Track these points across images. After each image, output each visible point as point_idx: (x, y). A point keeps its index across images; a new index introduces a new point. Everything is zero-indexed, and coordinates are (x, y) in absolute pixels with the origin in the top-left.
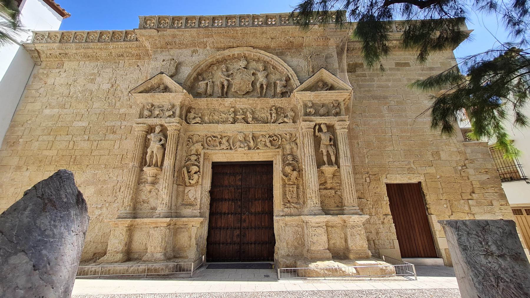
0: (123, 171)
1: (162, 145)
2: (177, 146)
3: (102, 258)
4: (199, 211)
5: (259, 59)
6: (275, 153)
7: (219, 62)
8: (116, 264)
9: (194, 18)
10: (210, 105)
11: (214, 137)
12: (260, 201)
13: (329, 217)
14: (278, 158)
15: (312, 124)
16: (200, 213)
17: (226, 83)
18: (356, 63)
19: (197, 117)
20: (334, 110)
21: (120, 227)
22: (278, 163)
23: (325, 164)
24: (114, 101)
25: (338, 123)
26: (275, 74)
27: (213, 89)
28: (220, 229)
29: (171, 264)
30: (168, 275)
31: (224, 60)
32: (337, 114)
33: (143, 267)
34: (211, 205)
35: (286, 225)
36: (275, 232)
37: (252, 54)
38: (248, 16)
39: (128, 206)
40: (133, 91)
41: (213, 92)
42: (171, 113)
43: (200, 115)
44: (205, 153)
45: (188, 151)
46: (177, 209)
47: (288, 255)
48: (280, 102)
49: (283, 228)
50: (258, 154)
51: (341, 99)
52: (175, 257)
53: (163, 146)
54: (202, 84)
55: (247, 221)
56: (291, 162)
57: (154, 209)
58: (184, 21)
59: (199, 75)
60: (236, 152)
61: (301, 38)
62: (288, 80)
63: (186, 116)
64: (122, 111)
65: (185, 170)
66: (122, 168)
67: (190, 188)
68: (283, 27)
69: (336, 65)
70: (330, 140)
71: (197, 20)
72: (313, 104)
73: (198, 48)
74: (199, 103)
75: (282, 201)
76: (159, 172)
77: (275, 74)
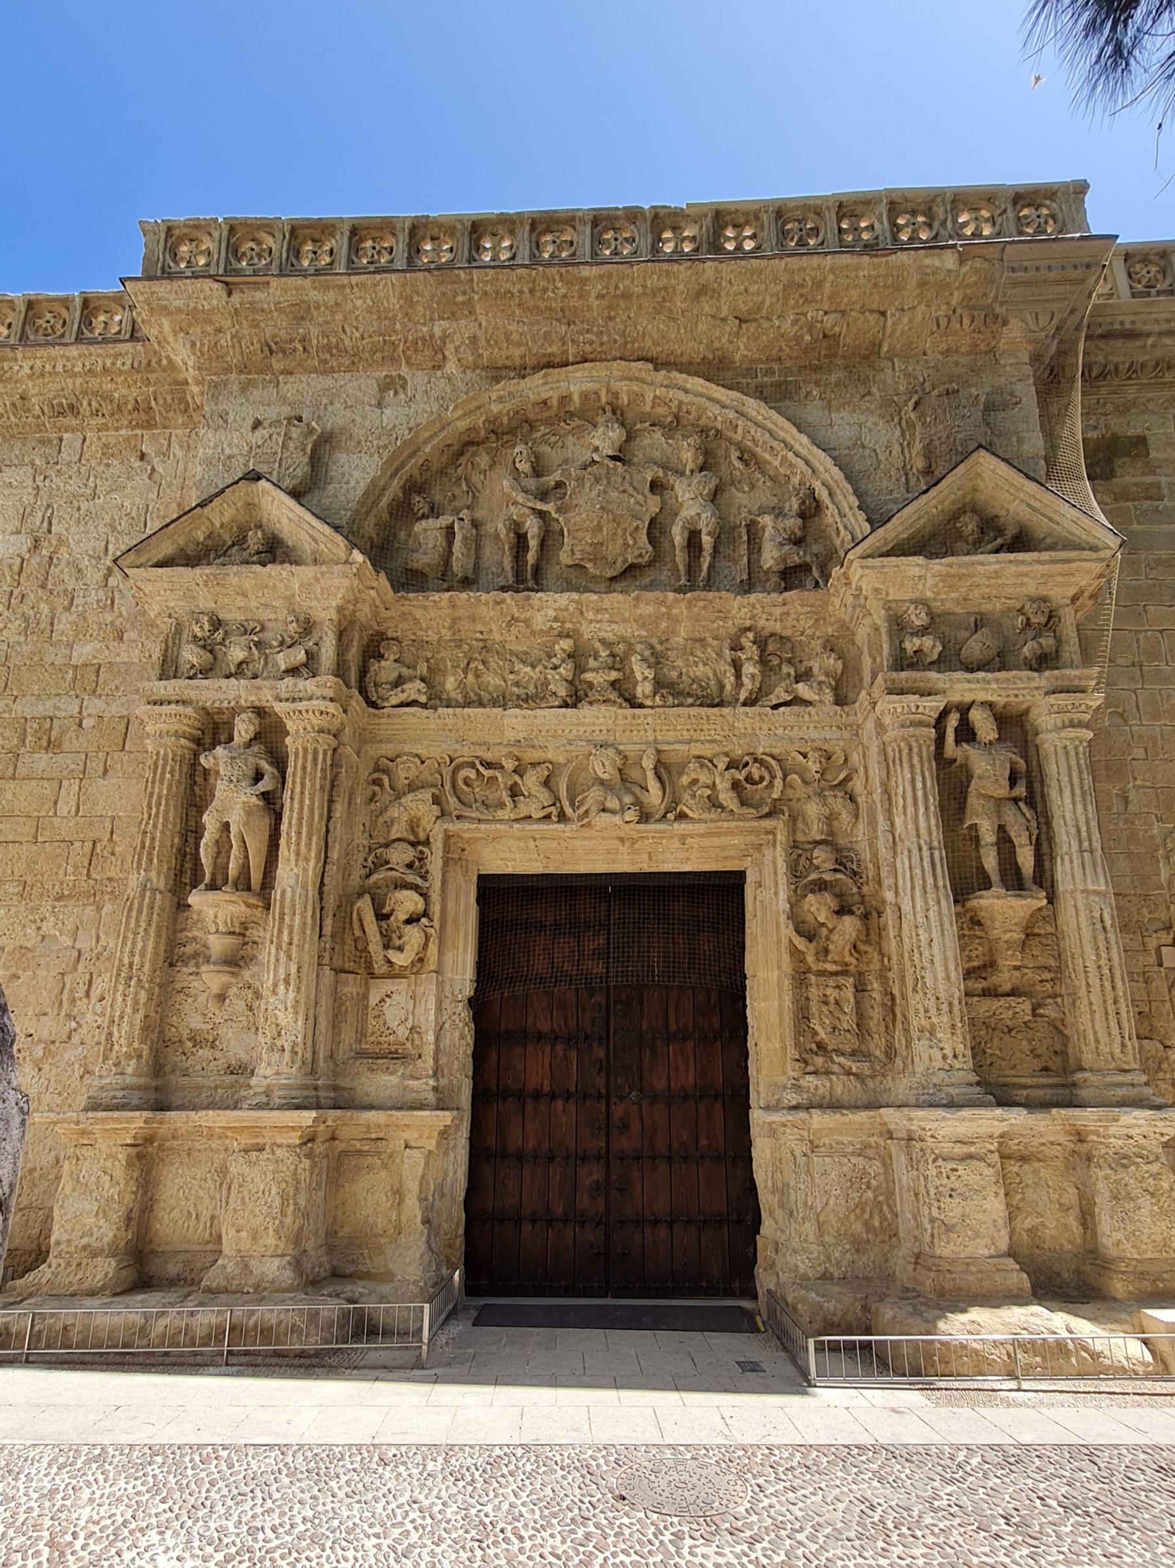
0: (99, 909)
1: (265, 796)
2: (331, 801)
3: (30, 1277)
4: (432, 1082)
5: (676, 416)
6: (752, 838)
7: (500, 433)
8: (89, 1302)
9: (387, 226)
10: (464, 625)
11: (488, 765)
12: (690, 1045)
13: (1016, 1118)
14: (768, 859)
15: (932, 706)
16: (435, 1089)
17: (532, 527)
18: (1115, 438)
19: (411, 679)
20: (1034, 641)
21: (103, 1145)
22: (768, 882)
23: (987, 884)
24: (45, 609)
25: (1052, 699)
26: (753, 487)
27: (478, 558)
28: (520, 1157)
29: (330, 1308)
30: (317, 1354)
31: (521, 425)
32: (1044, 661)
33: (207, 1317)
34: (479, 1056)
35: (814, 1147)
36: (761, 1176)
37: (649, 396)
38: (633, 215)
39: (129, 1056)
40: (132, 556)
41: (477, 567)
42: (301, 656)
43: (422, 668)
44: (448, 837)
45: (374, 824)
46: (336, 1075)
47: (826, 1277)
48: (777, 611)
49: (801, 1160)
50: (683, 839)
51: (1060, 594)
52: (337, 1275)
53: (271, 803)
54: (428, 531)
55: (635, 1127)
56: (828, 877)
57: (241, 1070)
58: (340, 243)
59: (415, 491)
60: (585, 832)
61: (872, 318)
62: (811, 509)
63: (363, 672)
64: (84, 652)
65: (365, 905)
66: (93, 896)
67: (389, 985)
68: (794, 263)
69: (1034, 443)
70: (1013, 780)
71: (403, 237)
72: (931, 615)
73: (404, 370)
74: (418, 614)
75: (789, 1044)
76: (258, 912)
77: (753, 487)
